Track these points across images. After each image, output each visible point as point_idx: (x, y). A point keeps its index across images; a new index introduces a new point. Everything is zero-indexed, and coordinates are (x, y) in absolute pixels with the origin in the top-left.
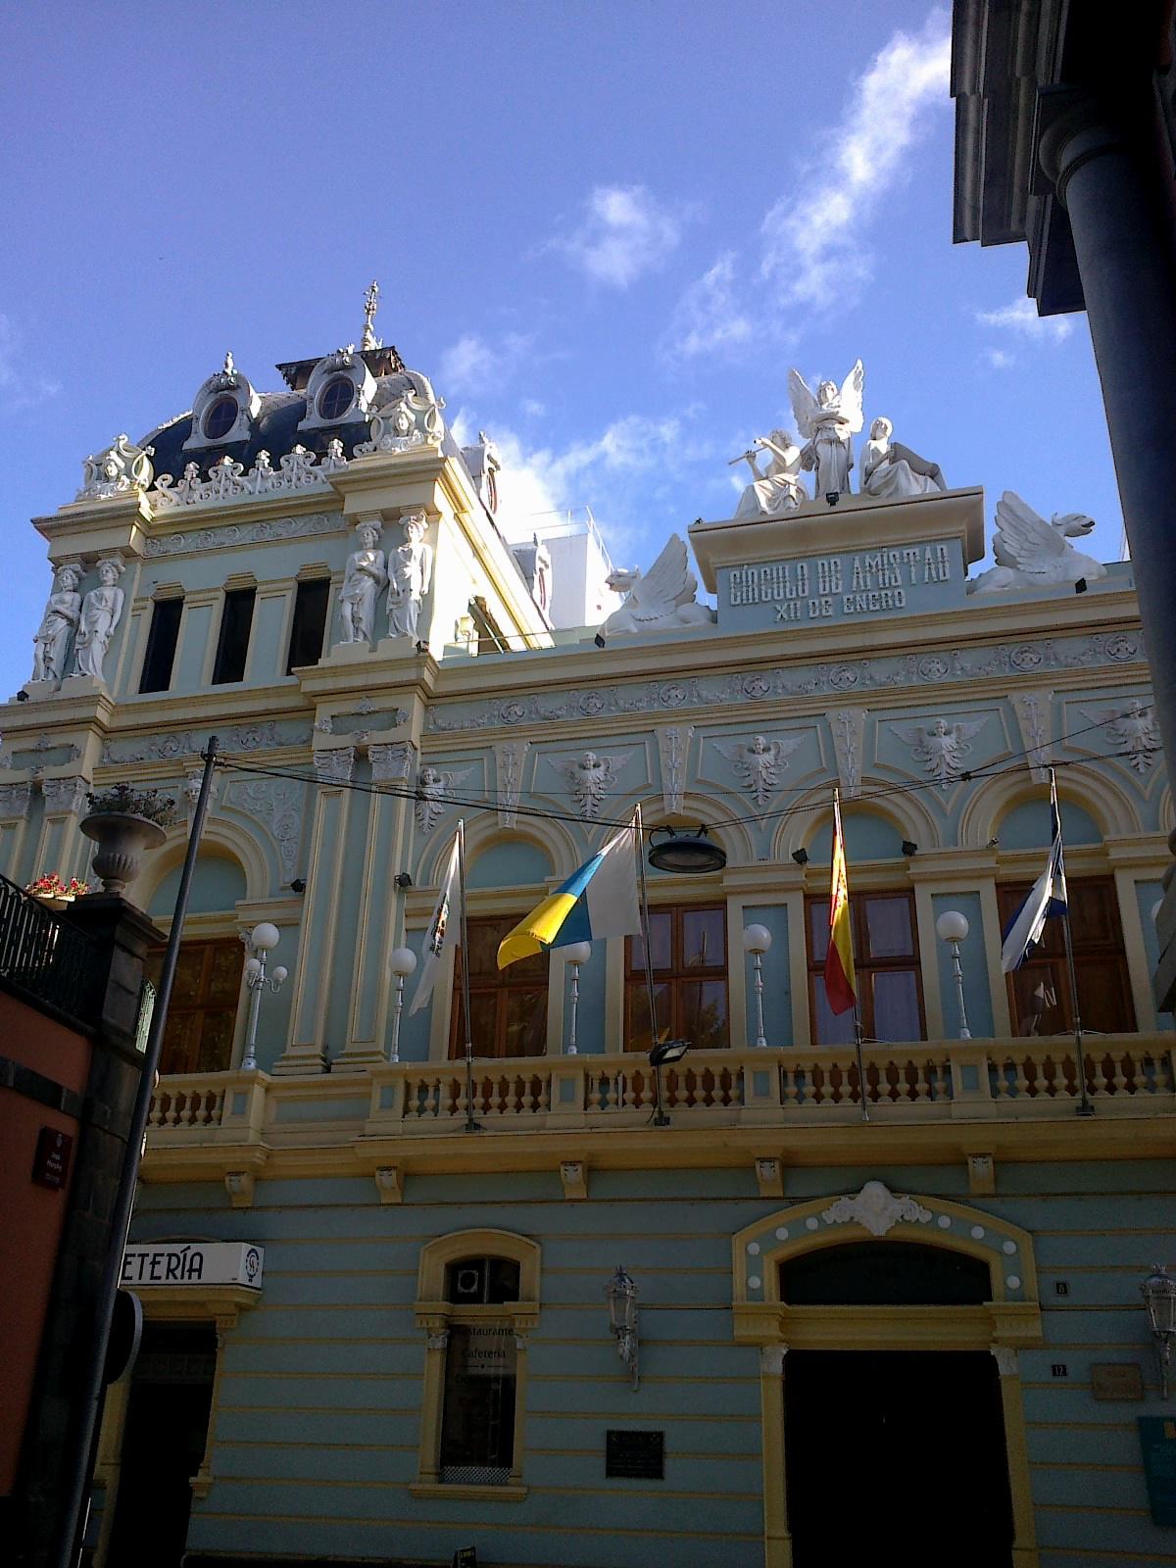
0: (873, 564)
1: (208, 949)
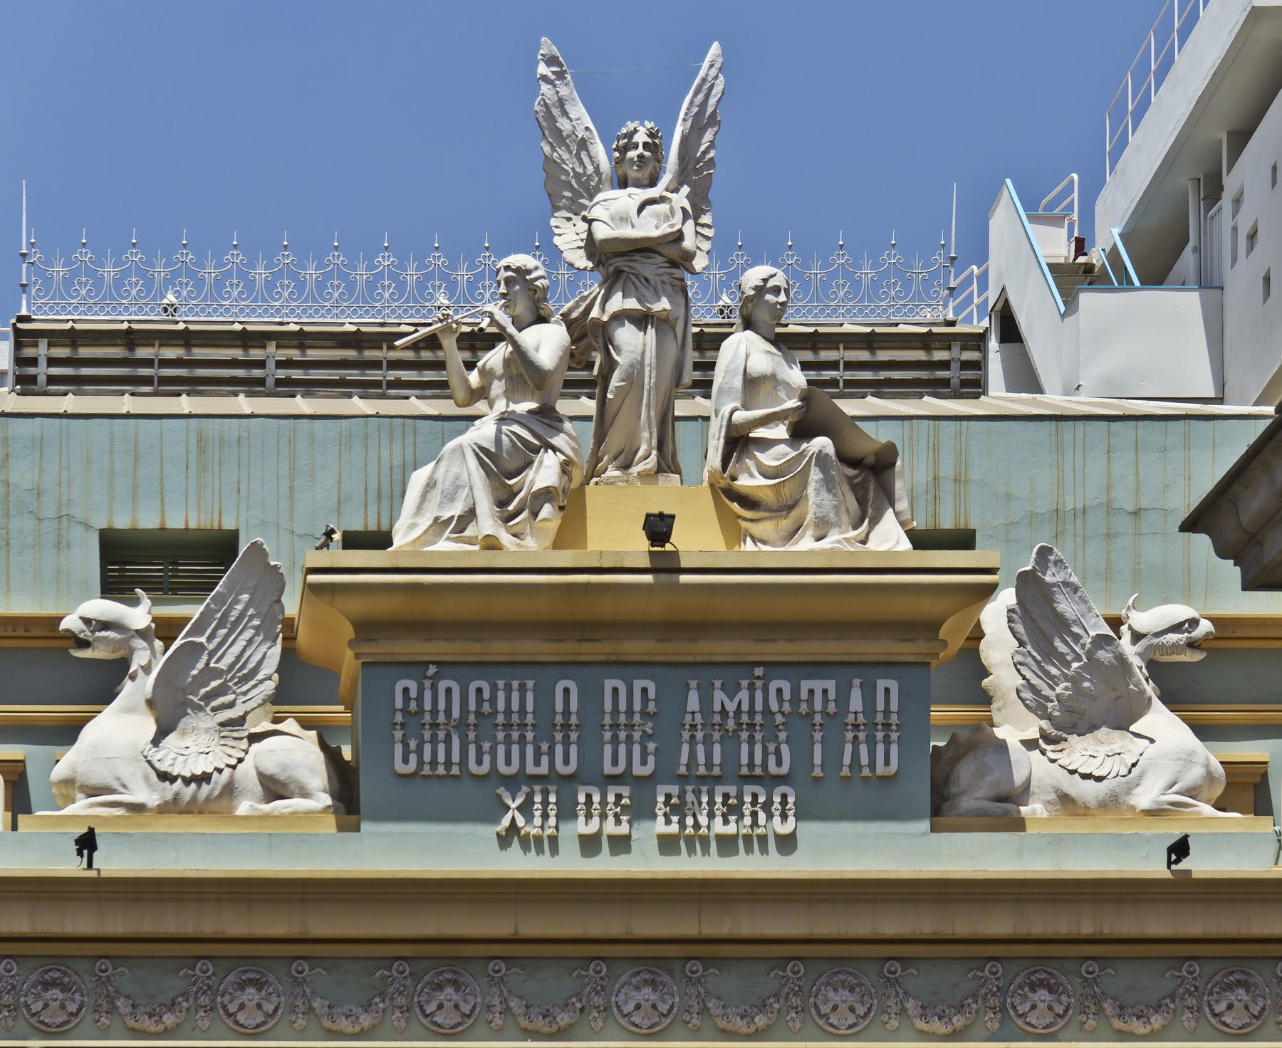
0: (731, 707)
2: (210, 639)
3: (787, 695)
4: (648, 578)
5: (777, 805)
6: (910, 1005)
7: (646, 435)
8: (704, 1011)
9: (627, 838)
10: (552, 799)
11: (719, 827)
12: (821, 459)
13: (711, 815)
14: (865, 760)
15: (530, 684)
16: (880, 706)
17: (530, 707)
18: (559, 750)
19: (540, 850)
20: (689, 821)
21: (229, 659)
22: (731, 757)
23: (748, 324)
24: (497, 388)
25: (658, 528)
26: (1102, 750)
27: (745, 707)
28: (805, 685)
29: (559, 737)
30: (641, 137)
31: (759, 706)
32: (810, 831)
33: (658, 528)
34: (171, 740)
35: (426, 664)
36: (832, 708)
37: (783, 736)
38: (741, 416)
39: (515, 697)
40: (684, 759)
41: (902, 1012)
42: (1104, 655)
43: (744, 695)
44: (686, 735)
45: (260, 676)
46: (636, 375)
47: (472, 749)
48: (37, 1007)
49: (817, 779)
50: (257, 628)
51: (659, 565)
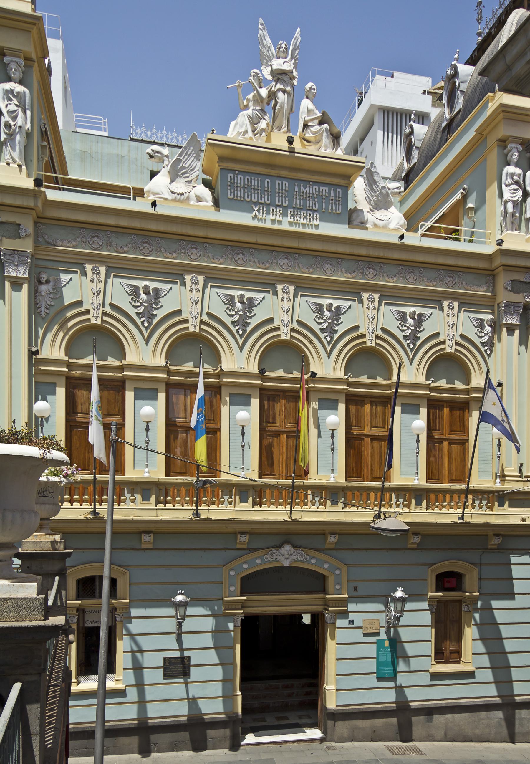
0: (305, 191)
1: (397, 179)
2: (183, 158)
3: (317, 190)
4: (288, 153)
5: (315, 217)
6: (343, 270)
7: (285, 122)
8: (298, 267)
9: (282, 221)
10: (265, 209)
11: (302, 221)
12: (326, 129)
13: (300, 218)
14: (334, 208)
15: (259, 179)
16: (338, 196)
17: (259, 185)
18: (266, 197)
19: (262, 222)
20: (296, 218)
21: (188, 164)
22: (305, 204)
23: (307, 98)
24: (251, 104)
25: (290, 141)
26: (383, 214)
27: (308, 192)
28: (321, 188)
29: (266, 193)
30: (283, 45)
31: (311, 192)
32: (322, 225)
33: (290, 141)
34: (174, 183)
35: (235, 170)
36: (327, 195)
37: (316, 200)
38: (307, 119)
39: (256, 181)
40: (294, 203)
41: (341, 271)
42: (384, 191)
43: (308, 189)
44: (295, 197)
45: (195, 170)
46: (282, 106)
47: (246, 194)
48: (141, 248)
49: (323, 212)
50: (195, 157)
51: (290, 150)
